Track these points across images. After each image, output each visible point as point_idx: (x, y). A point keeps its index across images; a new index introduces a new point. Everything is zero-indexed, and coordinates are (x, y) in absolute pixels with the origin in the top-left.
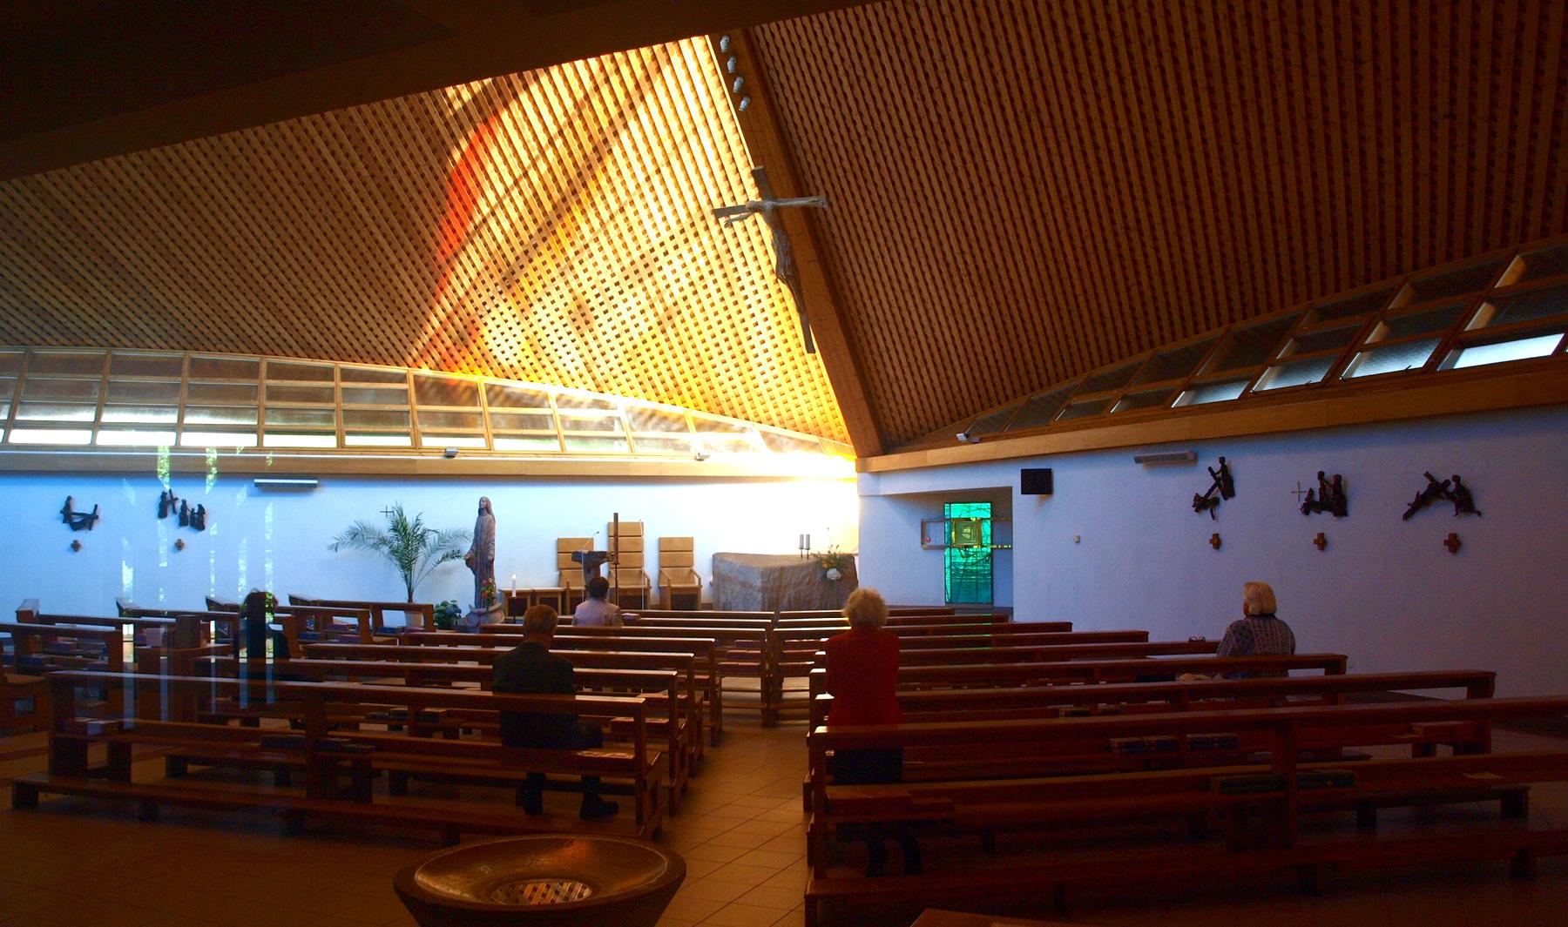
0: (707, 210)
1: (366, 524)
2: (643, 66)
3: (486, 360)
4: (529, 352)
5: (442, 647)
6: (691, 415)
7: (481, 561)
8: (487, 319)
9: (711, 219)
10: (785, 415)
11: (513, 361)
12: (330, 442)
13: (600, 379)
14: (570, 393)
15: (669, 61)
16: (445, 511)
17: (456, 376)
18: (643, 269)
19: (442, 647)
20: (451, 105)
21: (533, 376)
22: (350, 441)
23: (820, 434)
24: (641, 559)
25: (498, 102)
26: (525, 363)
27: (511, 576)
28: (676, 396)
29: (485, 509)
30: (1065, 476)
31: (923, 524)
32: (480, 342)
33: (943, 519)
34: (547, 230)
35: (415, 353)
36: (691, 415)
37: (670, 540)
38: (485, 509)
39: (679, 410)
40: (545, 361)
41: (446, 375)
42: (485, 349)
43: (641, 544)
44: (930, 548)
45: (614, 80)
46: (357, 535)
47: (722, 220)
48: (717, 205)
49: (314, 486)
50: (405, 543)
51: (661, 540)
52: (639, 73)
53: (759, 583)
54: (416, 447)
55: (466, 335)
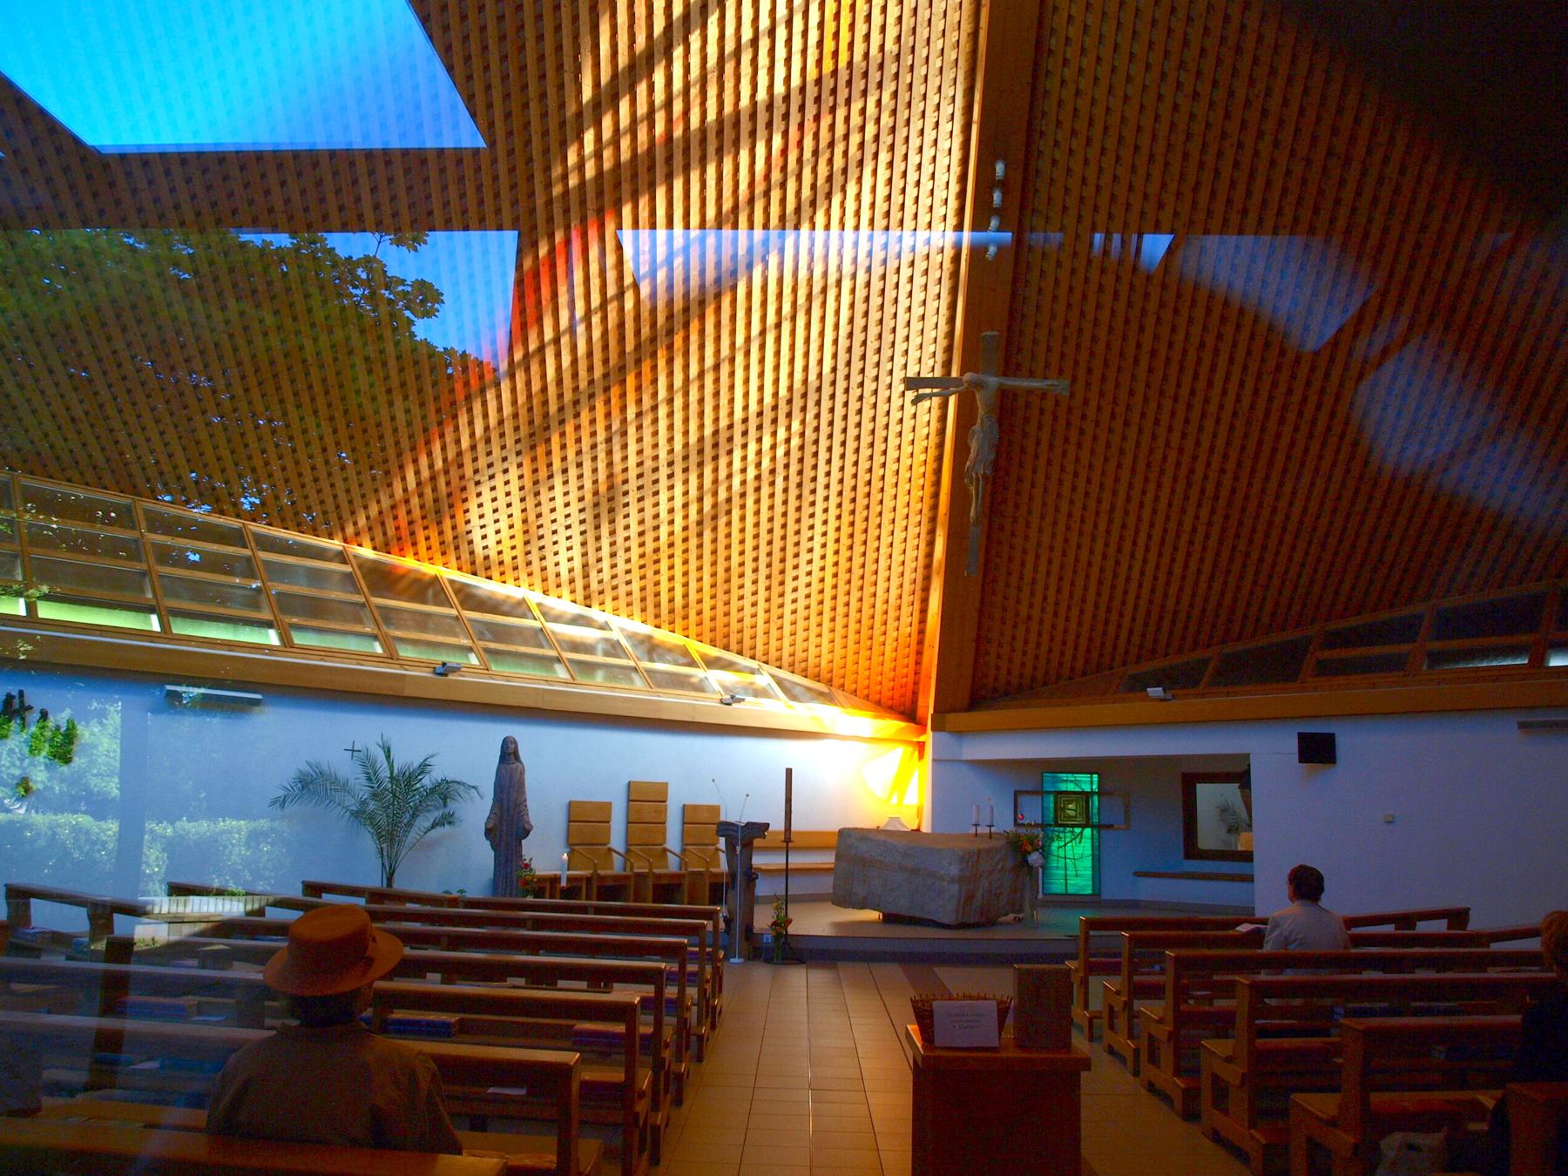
0: (899, 374)
1: (325, 768)
2: (814, 187)
3: (457, 546)
4: (519, 541)
5: (1421, 974)
6: (696, 648)
7: (508, 826)
8: (485, 489)
9: (899, 387)
10: (800, 655)
11: (492, 553)
12: (272, 638)
13: (594, 586)
14: (551, 602)
15: (843, 190)
16: (462, 752)
17: (409, 562)
18: (714, 447)
19: (1421, 974)
20: (565, 177)
21: (510, 575)
22: (299, 639)
23: (830, 682)
24: (664, 834)
25: (626, 188)
26: (507, 557)
27: (546, 854)
28: (678, 620)
29: (509, 753)
30: (1350, 740)
31: (1016, 794)
32: (460, 518)
33: (1041, 793)
34: (615, 375)
35: (362, 522)
36: (696, 648)
37: (696, 808)
38: (509, 753)
39: (676, 639)
40: (534, 557)
41: (393, 559)
42: (462, 528)
43: (664, 812)
44: (1127, 820)
45: (775, 195)
46: (312, 785)
47: (910, 395)
48: (911, 373)
49: (256, 703)
50: (402, 803)
51: (685, 808)
52: (806, 192)
53: (955, 870)
54: (391, 656)
55: (442, 509)
